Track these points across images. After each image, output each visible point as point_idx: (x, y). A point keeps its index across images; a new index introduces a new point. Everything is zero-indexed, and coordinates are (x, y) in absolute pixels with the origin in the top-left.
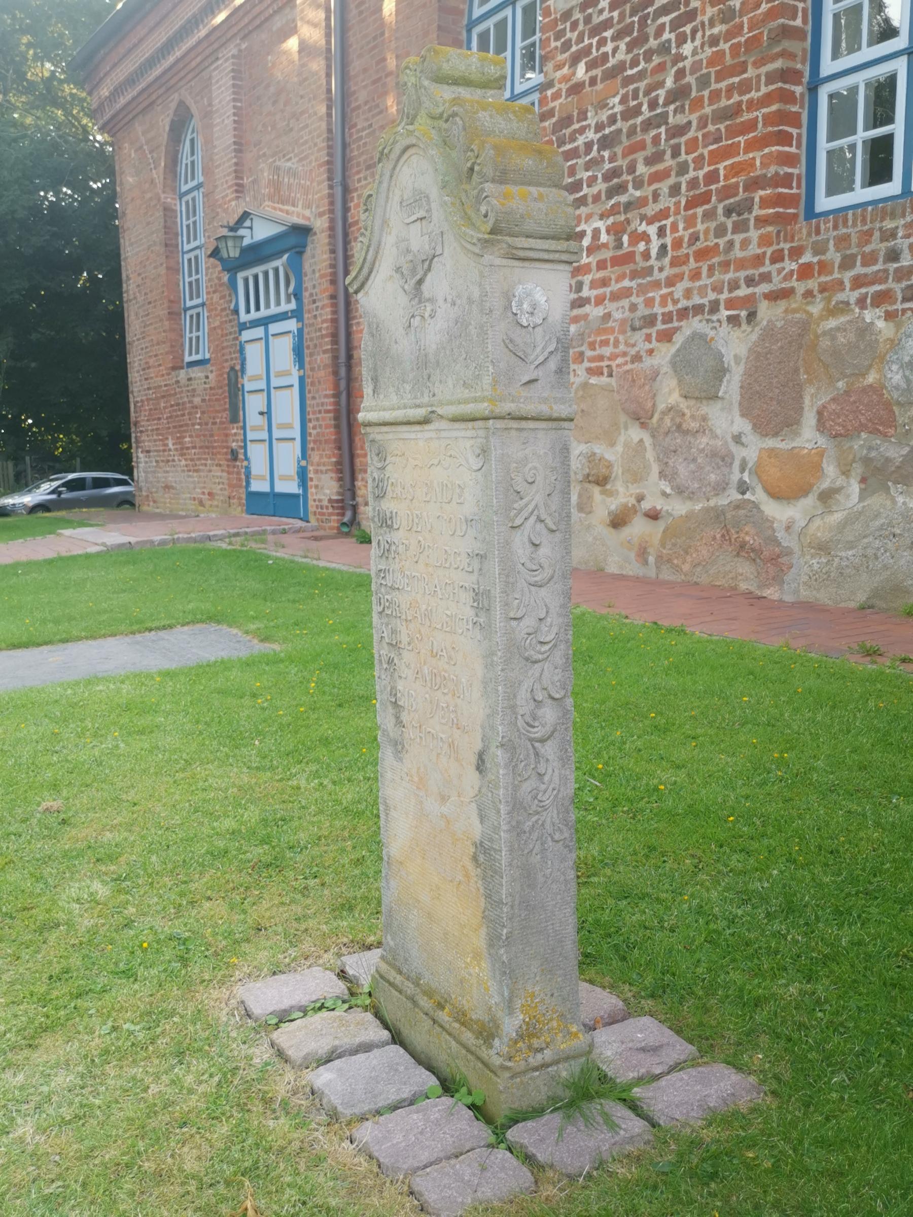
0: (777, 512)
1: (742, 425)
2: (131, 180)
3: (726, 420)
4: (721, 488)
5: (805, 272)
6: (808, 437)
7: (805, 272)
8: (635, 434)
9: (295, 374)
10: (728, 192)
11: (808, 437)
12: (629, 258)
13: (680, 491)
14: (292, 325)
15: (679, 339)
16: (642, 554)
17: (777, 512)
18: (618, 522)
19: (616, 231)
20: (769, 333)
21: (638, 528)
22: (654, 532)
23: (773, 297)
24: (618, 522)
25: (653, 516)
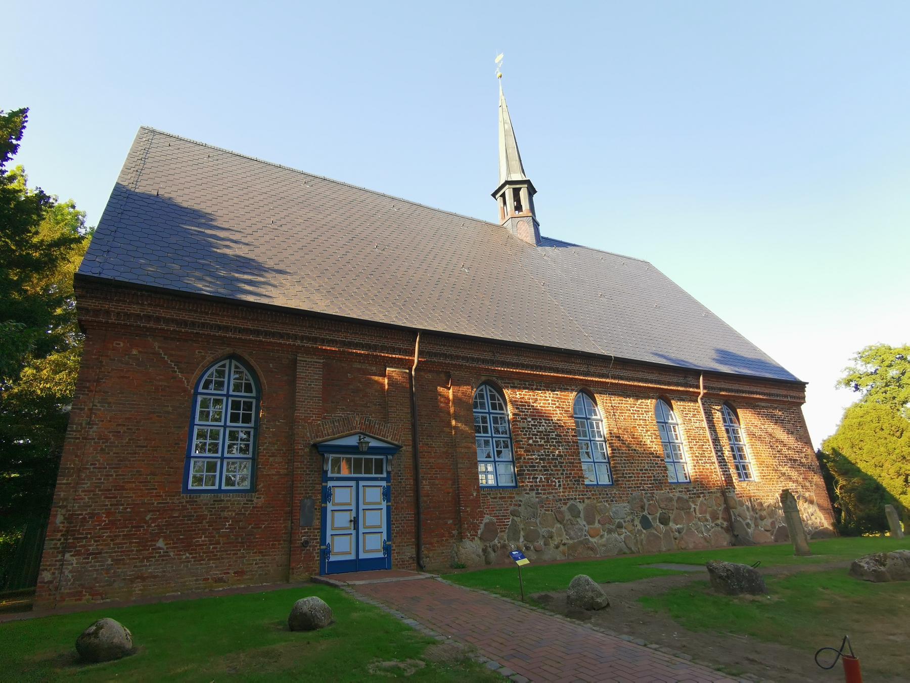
0: (592, 540)
1: (585, 523)
2: (450, 394)
3: (582, 522)
4: (581, 536)
5: (593, 495)
6: (597, 525)
7: (593, 495)
8: (559, 525)
9: (384, 505)
10: (574, 477)
11: (597, 525)
12: (551, 485)
13: (571, 538)
14: (384, 483)
15: (568, 505)
16: (564, 554)
17: (592, 540)
18: (557, 547)
19: (547, 479)
20: (588, 505)
21: (562, 548)
22: (565, 548)
23: (588, 498)
24: (557, 547)
25: (564, 544)
